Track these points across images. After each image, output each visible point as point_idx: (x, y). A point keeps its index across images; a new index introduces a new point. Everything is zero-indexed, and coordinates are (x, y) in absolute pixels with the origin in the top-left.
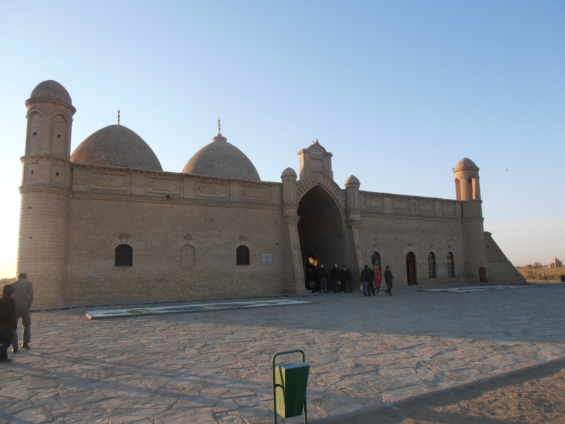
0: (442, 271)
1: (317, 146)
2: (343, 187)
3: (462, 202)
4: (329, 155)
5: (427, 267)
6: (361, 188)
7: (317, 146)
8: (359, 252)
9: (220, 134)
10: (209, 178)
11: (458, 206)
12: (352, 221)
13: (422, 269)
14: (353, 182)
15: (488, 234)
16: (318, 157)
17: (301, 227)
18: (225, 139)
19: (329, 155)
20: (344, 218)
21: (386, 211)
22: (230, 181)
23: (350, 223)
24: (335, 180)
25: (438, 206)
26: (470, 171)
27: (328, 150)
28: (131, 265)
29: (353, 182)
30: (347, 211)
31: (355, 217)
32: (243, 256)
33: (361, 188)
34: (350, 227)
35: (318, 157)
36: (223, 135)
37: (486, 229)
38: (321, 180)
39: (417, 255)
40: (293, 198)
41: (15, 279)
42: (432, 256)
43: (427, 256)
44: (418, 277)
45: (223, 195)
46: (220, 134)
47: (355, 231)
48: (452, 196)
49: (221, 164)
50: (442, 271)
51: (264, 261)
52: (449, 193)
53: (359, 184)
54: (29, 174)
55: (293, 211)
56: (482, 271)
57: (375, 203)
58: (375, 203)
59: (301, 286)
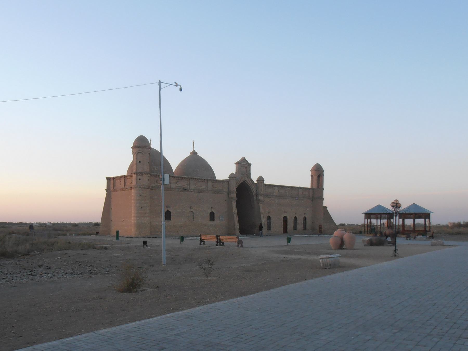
0: (300, 227)
1: (244, 160)
2: (255, 182)
3: (313, 189)
4: (250, 165)
5: (293, 224)
6: (265, 183)
7: (244, 160)
8: (262, 216)
9: (194, 150)
10: (199, 179)
11: (311, 191)
12: (259, 200)
13: (290, 226)
14: (261, 180)
15: (326, 207)
16: (244, 165)
17: (237, 203)
18: (197, 153)
19: (250, 165)
20: (255, 197)
21: (276, 194)
22: (207, 180)
23: (258, 201)
24: (252, 178)
25: (301, 191)
26: (318, 173)
27: (249, 162)
28: (170, 220)
29: (261, 180)
30: (257, 195)
31: (261, 198)
32: (212, 216)
33: (265, 183)
34: (258, 203)
35: (244, 165)
36: (196, 151)
37: (325, 204)
38: (246, 178)
39: (288, 218)
40: (234, 187)
41: (410, 226)
42: (296, 218)
43: (293, 219)
44: (288, 230)
45: (204, 187)
46: (194, 150)
47: (260, 205)
48: (309, 186)
49: (196, 167)
50: (300, 227)
51: (220, 220)
52: (308, 185)
53: (264, 181)
54: (139, 180)
55: (234, 195)
56: (320, 227)
57: (270, 190)
58: (270, 190)
59: (238, 232)
